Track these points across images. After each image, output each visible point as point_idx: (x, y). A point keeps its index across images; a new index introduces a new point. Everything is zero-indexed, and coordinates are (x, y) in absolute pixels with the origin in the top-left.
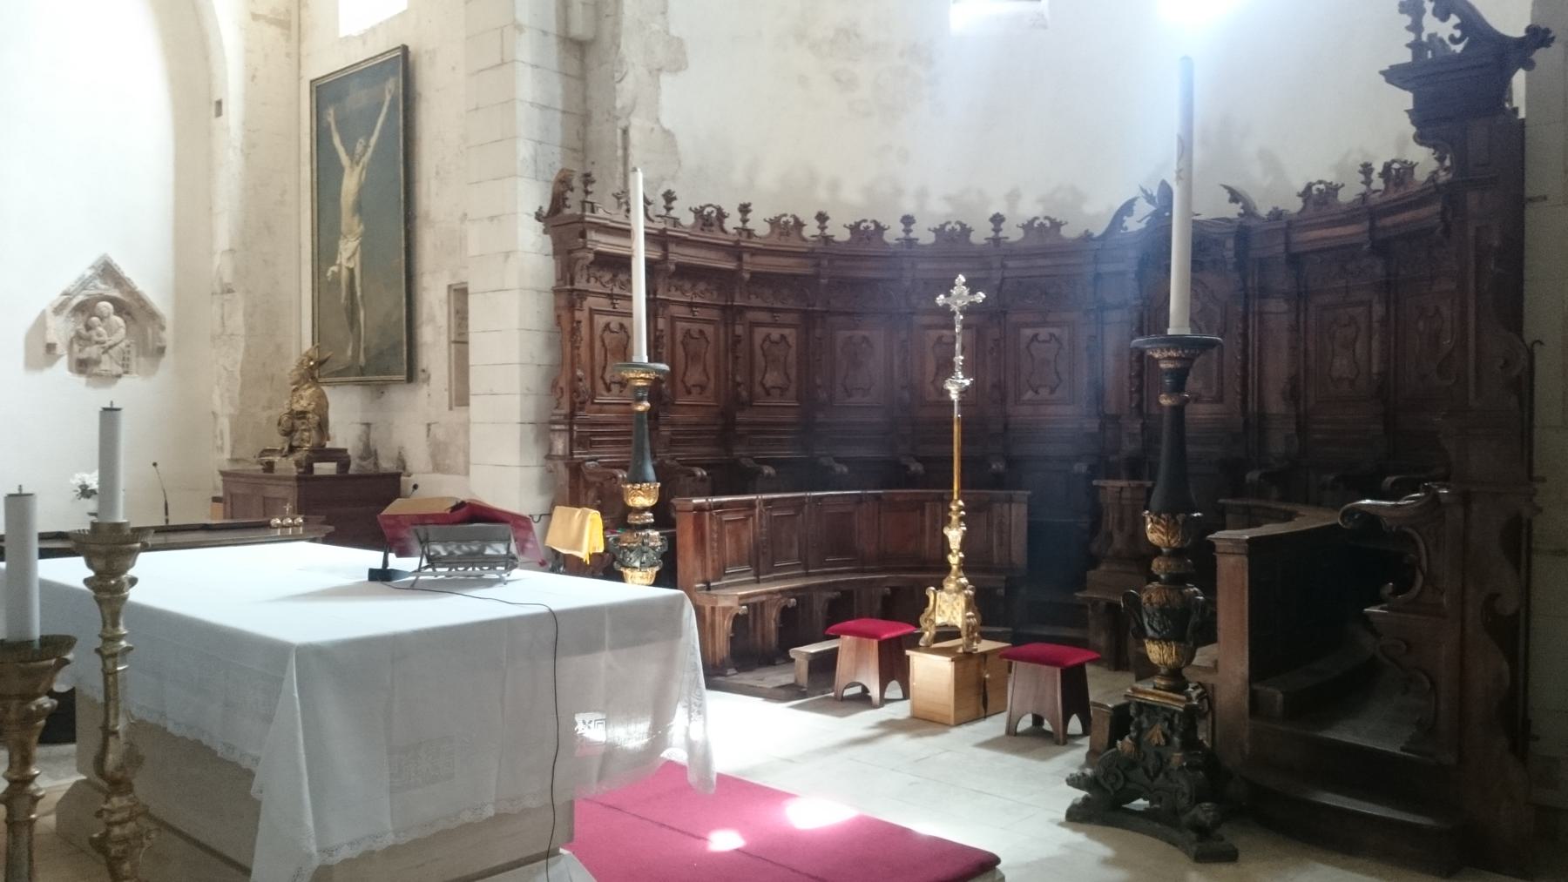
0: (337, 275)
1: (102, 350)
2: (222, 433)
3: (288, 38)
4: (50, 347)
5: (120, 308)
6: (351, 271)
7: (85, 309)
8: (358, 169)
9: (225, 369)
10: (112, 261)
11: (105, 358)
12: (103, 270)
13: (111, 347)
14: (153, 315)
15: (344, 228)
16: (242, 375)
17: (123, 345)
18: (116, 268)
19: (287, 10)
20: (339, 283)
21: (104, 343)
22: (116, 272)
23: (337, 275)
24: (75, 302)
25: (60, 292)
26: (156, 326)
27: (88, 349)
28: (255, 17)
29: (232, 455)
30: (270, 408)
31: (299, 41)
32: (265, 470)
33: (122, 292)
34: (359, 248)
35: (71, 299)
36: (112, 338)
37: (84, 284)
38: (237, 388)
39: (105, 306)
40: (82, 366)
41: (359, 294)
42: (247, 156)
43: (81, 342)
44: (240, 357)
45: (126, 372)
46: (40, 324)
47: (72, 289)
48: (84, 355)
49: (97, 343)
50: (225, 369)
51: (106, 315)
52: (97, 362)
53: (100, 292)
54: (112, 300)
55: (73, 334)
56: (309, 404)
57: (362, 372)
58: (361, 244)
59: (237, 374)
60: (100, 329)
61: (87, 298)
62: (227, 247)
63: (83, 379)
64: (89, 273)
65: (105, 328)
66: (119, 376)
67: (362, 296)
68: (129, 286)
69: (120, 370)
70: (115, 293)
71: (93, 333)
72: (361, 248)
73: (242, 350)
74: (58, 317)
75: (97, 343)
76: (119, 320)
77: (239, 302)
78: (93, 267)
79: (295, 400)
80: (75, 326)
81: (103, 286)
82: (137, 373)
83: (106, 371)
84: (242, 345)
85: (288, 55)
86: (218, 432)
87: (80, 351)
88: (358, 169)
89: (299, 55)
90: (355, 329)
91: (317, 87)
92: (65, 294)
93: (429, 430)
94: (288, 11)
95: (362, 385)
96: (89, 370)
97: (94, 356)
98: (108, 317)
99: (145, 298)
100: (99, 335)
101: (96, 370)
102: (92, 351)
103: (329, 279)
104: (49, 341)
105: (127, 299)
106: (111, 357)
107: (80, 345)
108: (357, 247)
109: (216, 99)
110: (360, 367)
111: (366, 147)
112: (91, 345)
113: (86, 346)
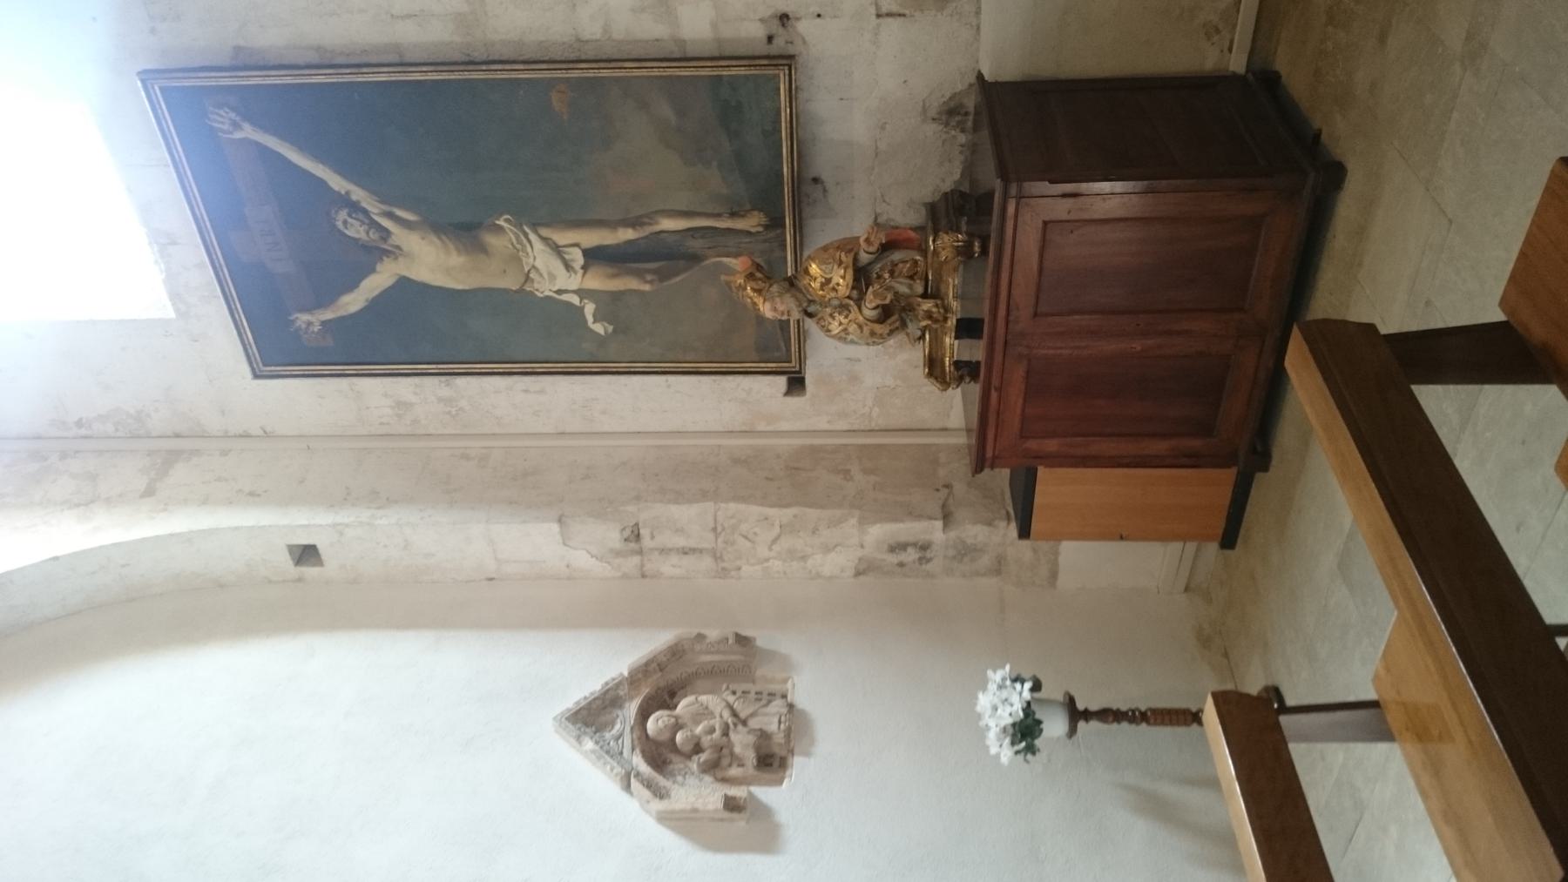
0: (610, 304)
1: (740, 727)
2: (898, 547)
3: (196, 452)
4: (732, 805)
5: (664, 698)
6: (594, 256)
7: (660, 755)
8: (400, 236)
9: (775, 541)
10: (569, 710)
11: (754, 723)
12: (587, 725)
13: (735, 714)
14: (676, 652)
15: (510, 282)
16: (787, 506)
17: (731, 699)
18: (583, 703)
19: (148, 455)
20: (616, 296)
21: (727, 725)
22: (590, 703)
23: (610, 304)
24: (644, 768)
25: (624, 796)
26: (698, 647)
27: (737, 750)
28: (149, 492)
29: (936, 519)
30: (847, 472)
31: (204, 436)
32: (974, 376)
33: (632, 698)
34: (545, 232)
35: (638, 775)
36: (717, 711)
37: (611, 753)
38: (813, 513)
39: (656, 723)
40: (771, 762)
41: (627, 234)
42: (390, 502)
43: (725, 762)
44: (755, 510)
45: (784, 696)
46: (684, 823)
47: (618, 769)
48: (750, 757)
49: (726, 733)
50: (775, 541)
51: (673, 720)
52: (764, 736)
53: (628, 730)
54: (644, 715)
55: (708, 779)
56: (840, 263)
57: (776, 223)
58: (535, 226)
59: (790, 512)
60: (699, 730)
61: (638, 751)
62: (555, 527)
63: (798, 763)
64: (589, 744)
65: (697, 723)
66: (791, 706)
67: (634, 223)
68: (618, 685)
69: (777, 706)
70: (632, 709)
71: (706, 741)
72: (547, 225)
73: (742, 507)
74: (673, 794)
75: (726, 733)
76: (684, 705)
77: (650, 513)
78: (578, 738)
79: (833, 294)
80: (693, 774)
81: (618, 726)
82: (785, 681)
83: (780, 722)
84: (733, 506)
85: (224, 453)
86: (893, 559)
87: (741, 765)
88: (400, 236)
89: (226, 436)
90: (696, 245)
91: (265, 365)
92: (627, 787)
93: (889, 15)
94: (150, 453)
95: (805, 341)
96: (776, 750)
97: (751, 739)
98: (677, 718)
99: (644, 661)
100: (712, 730)
101: (779, 738)
102: (742, 742)
103: (610, 328)
104: (720, 805)
105: (645, 691)
106: (752, 715)
107: (730, 765)
108: (545, 240)
109: (285, 561)
110: (767, 227)
111: (355, 208)
112: (730, 745)
113: (732, 754)
